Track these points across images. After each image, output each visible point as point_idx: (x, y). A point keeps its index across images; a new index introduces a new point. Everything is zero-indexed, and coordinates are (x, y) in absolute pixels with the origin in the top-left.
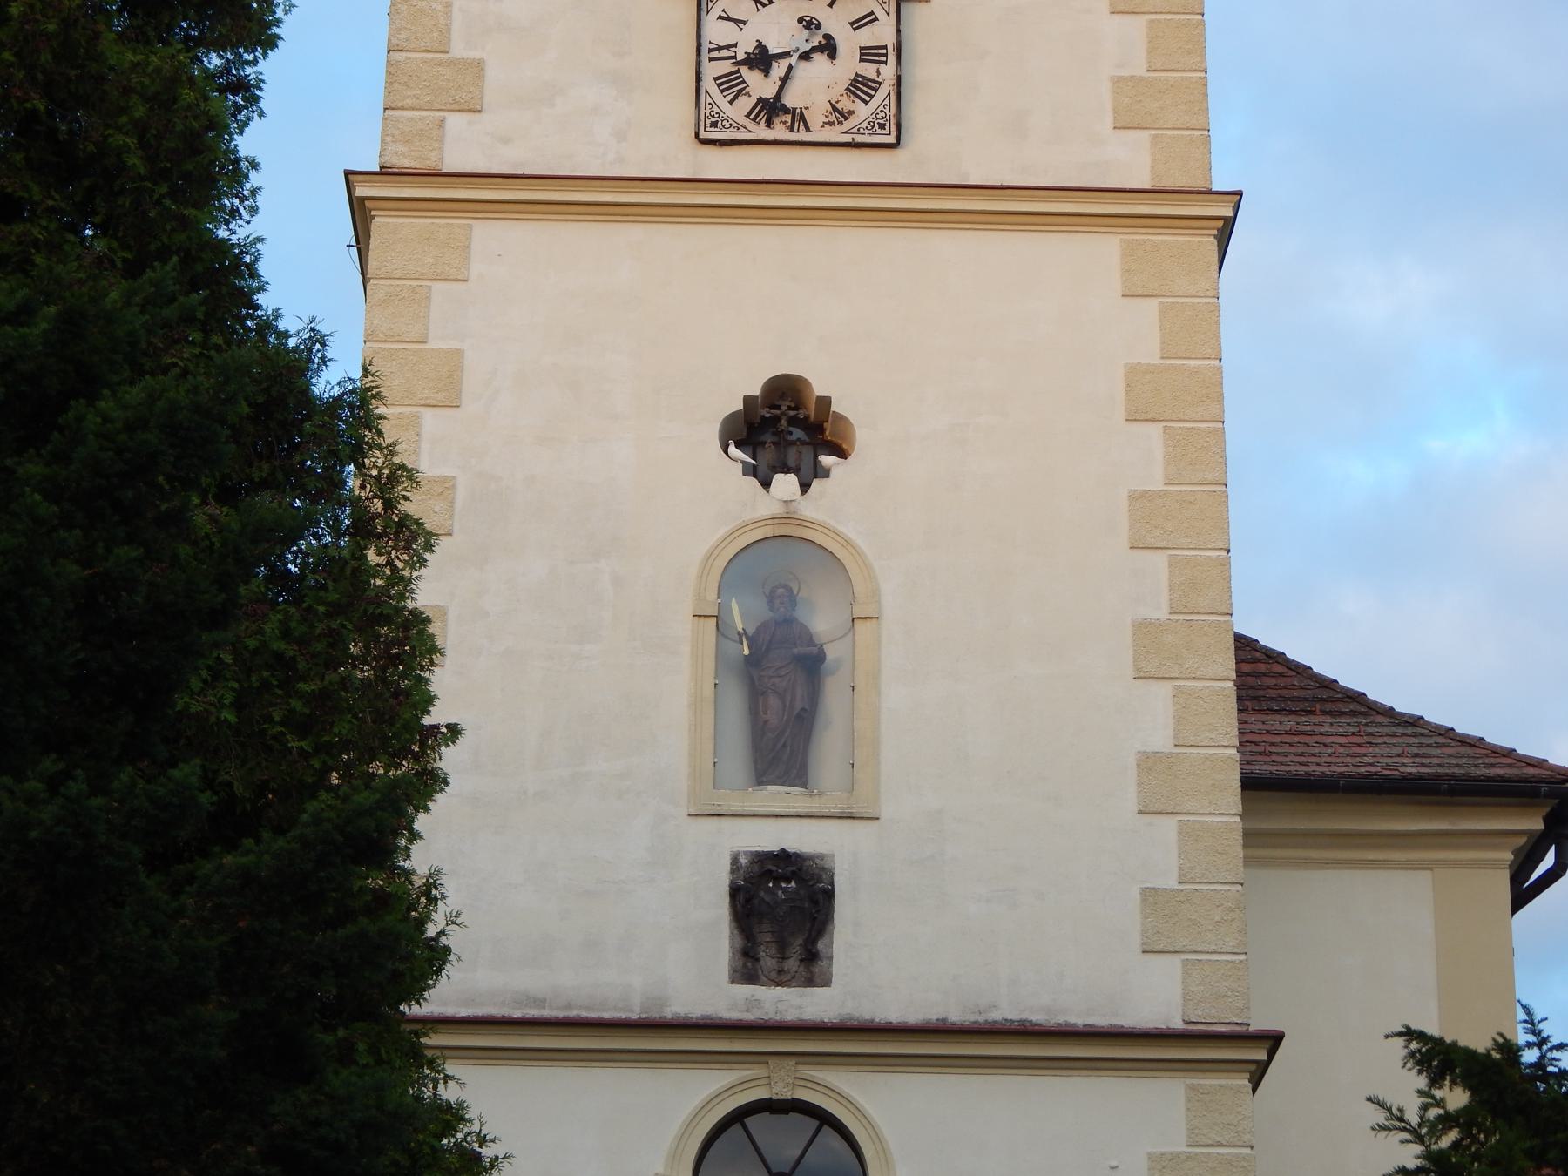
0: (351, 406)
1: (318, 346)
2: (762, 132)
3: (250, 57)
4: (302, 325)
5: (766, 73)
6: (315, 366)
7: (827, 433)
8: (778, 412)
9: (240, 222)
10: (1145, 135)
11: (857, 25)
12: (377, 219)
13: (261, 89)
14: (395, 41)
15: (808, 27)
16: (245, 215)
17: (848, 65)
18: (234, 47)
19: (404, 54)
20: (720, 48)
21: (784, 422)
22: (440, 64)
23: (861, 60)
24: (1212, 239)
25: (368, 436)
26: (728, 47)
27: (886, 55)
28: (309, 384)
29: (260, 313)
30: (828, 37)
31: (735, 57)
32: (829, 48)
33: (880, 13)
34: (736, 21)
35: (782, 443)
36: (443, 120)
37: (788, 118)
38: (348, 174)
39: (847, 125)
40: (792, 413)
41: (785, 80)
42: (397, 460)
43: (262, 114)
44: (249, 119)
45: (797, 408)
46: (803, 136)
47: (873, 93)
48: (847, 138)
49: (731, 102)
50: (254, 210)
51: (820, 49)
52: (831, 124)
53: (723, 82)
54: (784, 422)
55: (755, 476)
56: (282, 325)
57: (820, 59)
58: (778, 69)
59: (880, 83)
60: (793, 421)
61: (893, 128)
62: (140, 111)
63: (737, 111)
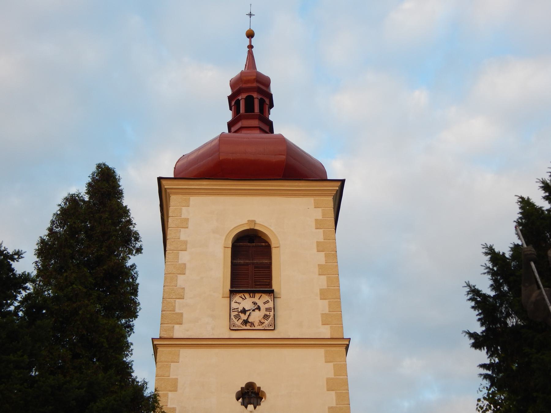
0: (153, 398)
1: (145, 385)
2: (244, 327)
3: (131, 320)
4: (142, 380)
5: (245, 314)
6: (145, 389)
7: (260, 395)
8: (248, 391)
9: (128, 357)
10: (329, 326)
11: (265, 303)
12: (159, 349)
13: (134, 327)
14: (163, 309)
15: (254, 304)
16: (130, 355)
17: (263, 312)
18: (128, 318)
19: (165, 312)
20: (235, 309)
21: (250, 393)
22: (173, 314)
23: (266, 311)
24: (344, 349)
25: (156, 405)
26: (236, 309)
27: (271, 310)
28: (143, 393)
29: (132, 377)
30: (258, 306)
31: (238, 311)
32: (259, 308)
33: (270, 300)
34: (238, 303)
35: (250, 398)
36: (174, 326)
37: (250, 324)
38: (152, 339)
39: (263, 325)
40: (252, 391)
41: (249, 315)
42: (163, 410)
43: (134, 333)
44: (131, 334)
45: (253, 389)
46: (253, 328)
47: (268, 318)
48: (263, 328)
49: (237, 321)
50: (132, 354)
51: (257, 309)
52: (260, 325)
53: (236, 317)
54: (250, 393)
55: (244, 405)
56: (137, 380)
57: (257, 311)
58: (248, 313)
59: (270, 316)
60: (252, 393)
61: (273, 326)
62: (107, 334)
63: (239, 323)
